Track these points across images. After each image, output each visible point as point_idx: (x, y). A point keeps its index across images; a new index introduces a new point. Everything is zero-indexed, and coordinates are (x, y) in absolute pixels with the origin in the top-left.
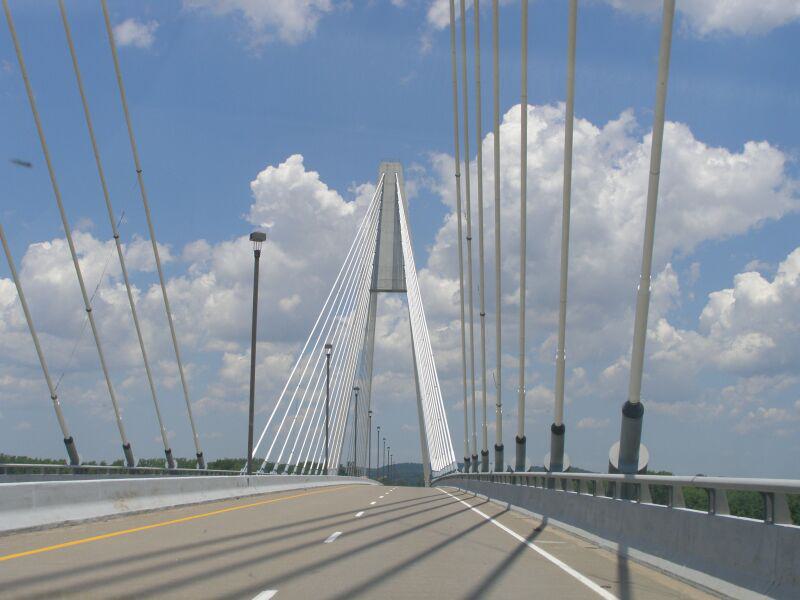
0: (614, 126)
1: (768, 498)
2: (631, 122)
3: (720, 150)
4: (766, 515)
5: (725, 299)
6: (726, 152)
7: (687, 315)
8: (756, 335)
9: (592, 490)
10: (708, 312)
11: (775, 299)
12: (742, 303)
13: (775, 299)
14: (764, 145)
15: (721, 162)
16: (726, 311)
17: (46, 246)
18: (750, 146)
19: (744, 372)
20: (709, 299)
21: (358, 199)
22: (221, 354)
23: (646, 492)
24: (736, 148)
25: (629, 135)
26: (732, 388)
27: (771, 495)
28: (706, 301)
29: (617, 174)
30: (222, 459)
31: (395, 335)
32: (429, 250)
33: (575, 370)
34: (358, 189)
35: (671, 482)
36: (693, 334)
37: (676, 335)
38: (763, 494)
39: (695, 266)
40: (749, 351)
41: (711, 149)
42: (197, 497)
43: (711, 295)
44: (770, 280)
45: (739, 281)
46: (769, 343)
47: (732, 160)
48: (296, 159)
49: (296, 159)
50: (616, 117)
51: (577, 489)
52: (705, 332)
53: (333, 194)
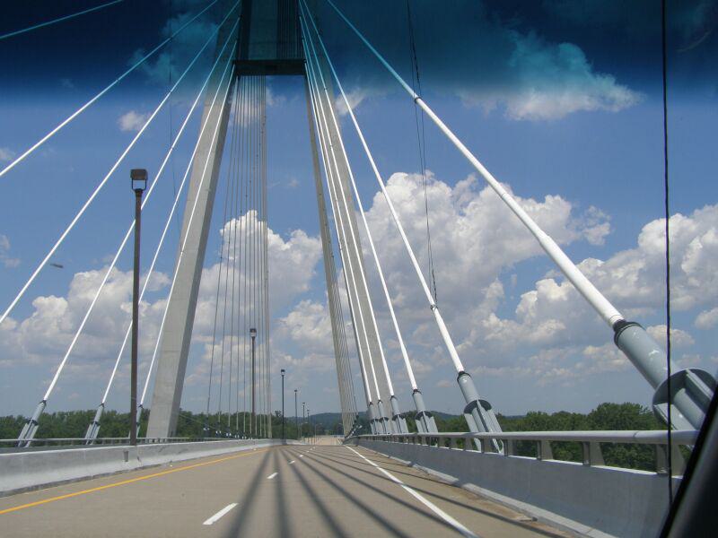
0: (463, 184)
1: (585, 445)
2: (475, 182)
3: (530, 200)
4: (655, 462)
5: (531, 298)
6: (534, 202)
7: (507, 309)
8: (553, 321)
9: (420, 442)
10: (520, 307)
11: (565, 299)
12: (542, 300)
13: (565, 299)
14: (558, 198)
15: (531, 208)
16: (533, 307)
17: (87, 275)
18: (549, 198)
19: (545, 346)
20: (521, 299)
21: (292, 240)
22: (204, 344)
23: (424, 440)
24: (541, 200)
25: (472, 191)
26: (536, 357)
27: (588, 444)
28: (519, 300)
29: (464, 219)
30: (577, 413)
31: (317, 329)
32: (315, 272)
33: (436, 349)
34: (292, 234)
35: (540, 437)
36: (512, 322)
37: (501, 324)
38: (581, 443)
39: (514, 277)
40: (549, 332)
41: (524, 200)
42: (233, 449)
43: (522, 296)
44: (559, 285)
45: (539, 286)
46: (562, 326)
47: (539, 207)
48: (252, 213)
49: (252, 213)
50: (464, 178)
51: (414, 442)
52: (520, 320)
53: (277, 236)
